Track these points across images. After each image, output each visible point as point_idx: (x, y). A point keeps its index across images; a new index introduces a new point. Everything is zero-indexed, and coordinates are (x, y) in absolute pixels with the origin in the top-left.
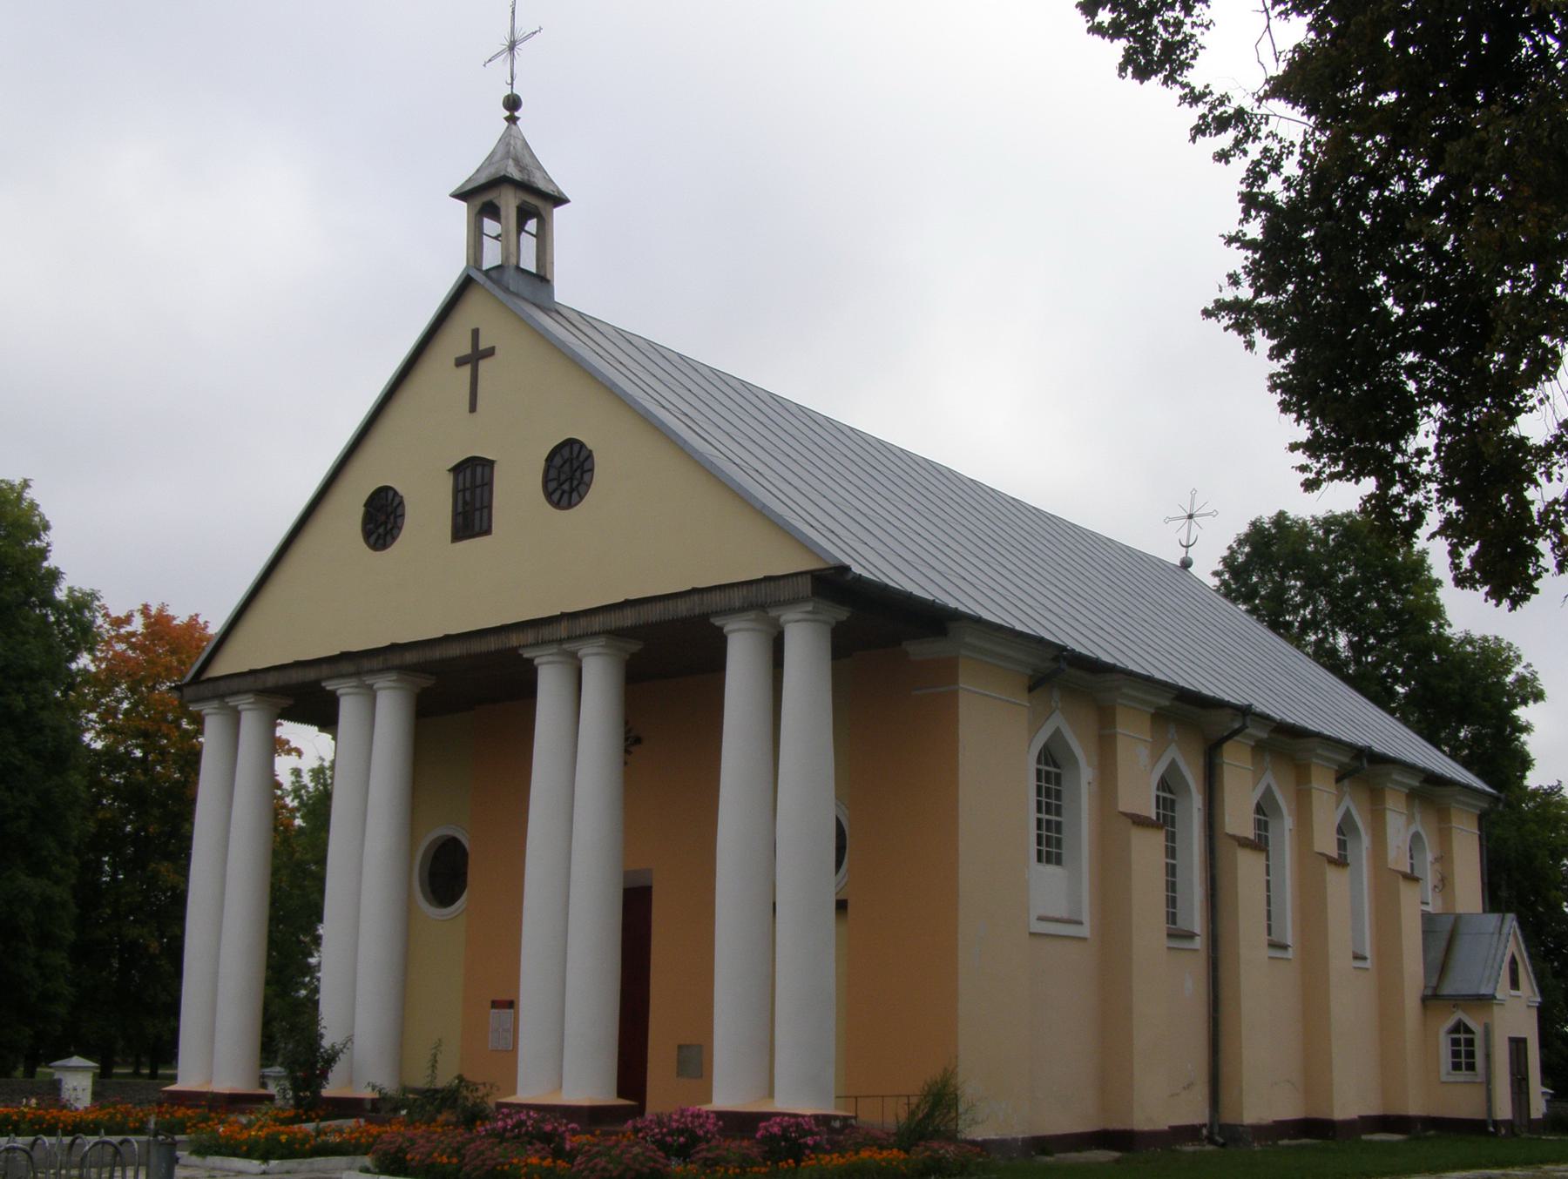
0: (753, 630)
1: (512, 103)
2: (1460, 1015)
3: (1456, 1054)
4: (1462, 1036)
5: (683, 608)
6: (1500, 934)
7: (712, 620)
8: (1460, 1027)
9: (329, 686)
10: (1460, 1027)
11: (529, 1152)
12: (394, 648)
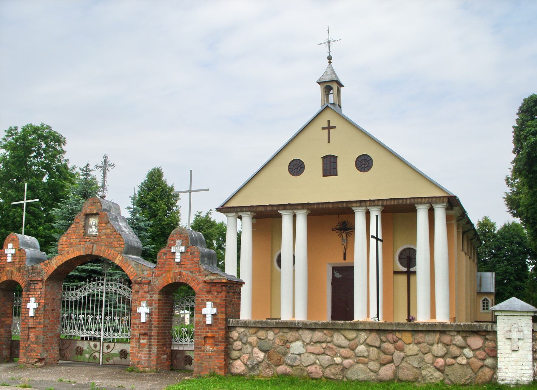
0: (426, 208)
1: (330, 58)
2: (485, 297)
3: (484, 306)
4: (486, 302)
5: (408, 202)
6: (492, 277)
7: (415, 205)
8: (485, 300)
9: (280, 212)
10: (485, 300)
11: (516, 326)
12: (308, 204)
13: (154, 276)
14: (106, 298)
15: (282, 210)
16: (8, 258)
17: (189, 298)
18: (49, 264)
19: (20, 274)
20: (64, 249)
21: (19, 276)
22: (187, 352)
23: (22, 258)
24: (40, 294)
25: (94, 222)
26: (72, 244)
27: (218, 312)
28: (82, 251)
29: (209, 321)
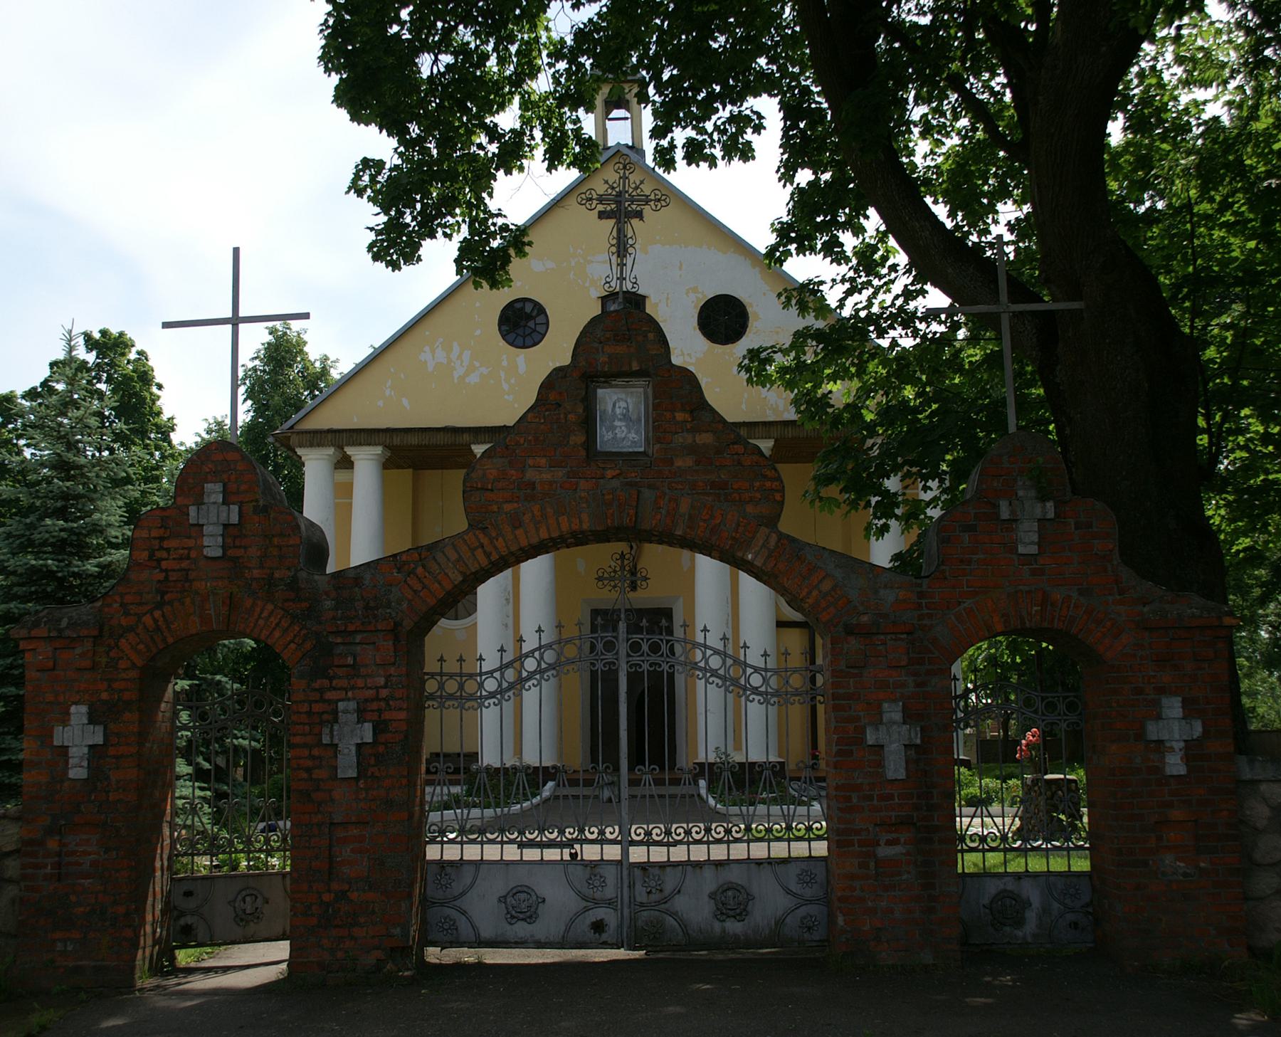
0: (372, 459)
13: (928, 608)
14: (836, 708)
15: (353, 444)
16: (206, 541)
17: (662, 640)
18: (424, 566)
19: (270, 607)
20: (495, 508)
21: (265, 614)
22: (1024, 860)
23: (276, 541)
24: (385, 686)
25: (623, 404)
26: (534, 489)
27: (1206, 732)
28: (585, 517)
29: (1175, 764)
